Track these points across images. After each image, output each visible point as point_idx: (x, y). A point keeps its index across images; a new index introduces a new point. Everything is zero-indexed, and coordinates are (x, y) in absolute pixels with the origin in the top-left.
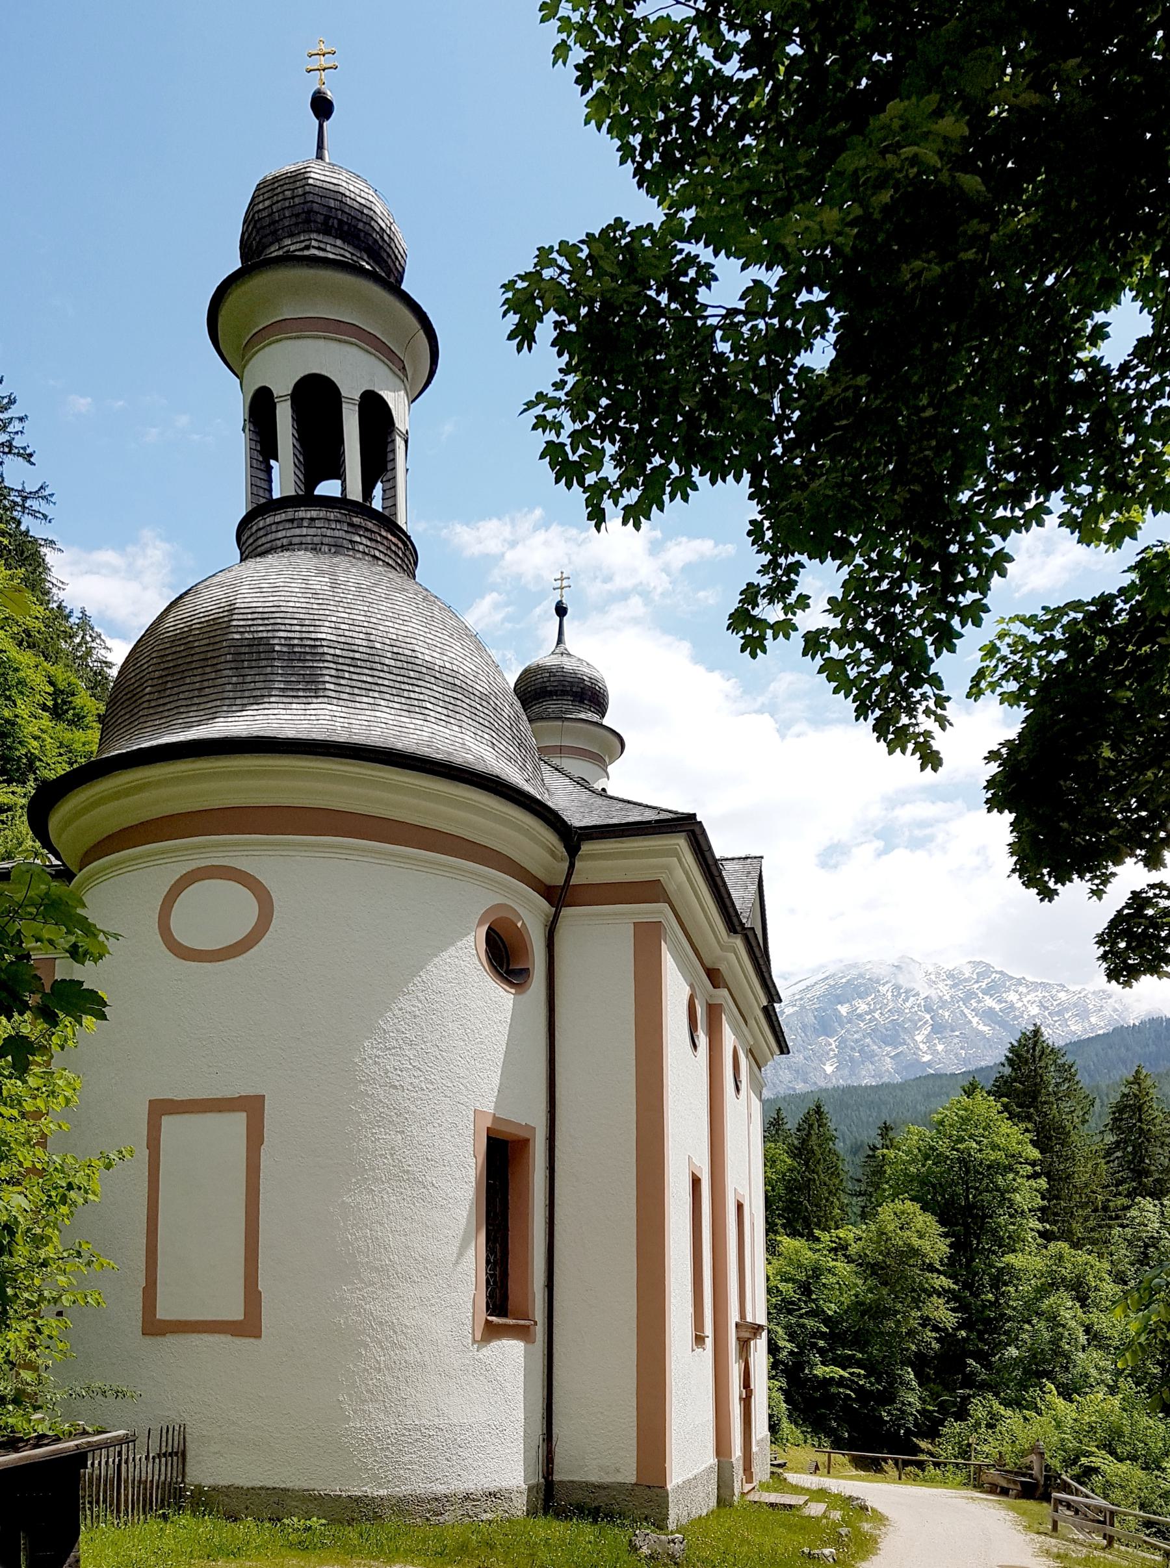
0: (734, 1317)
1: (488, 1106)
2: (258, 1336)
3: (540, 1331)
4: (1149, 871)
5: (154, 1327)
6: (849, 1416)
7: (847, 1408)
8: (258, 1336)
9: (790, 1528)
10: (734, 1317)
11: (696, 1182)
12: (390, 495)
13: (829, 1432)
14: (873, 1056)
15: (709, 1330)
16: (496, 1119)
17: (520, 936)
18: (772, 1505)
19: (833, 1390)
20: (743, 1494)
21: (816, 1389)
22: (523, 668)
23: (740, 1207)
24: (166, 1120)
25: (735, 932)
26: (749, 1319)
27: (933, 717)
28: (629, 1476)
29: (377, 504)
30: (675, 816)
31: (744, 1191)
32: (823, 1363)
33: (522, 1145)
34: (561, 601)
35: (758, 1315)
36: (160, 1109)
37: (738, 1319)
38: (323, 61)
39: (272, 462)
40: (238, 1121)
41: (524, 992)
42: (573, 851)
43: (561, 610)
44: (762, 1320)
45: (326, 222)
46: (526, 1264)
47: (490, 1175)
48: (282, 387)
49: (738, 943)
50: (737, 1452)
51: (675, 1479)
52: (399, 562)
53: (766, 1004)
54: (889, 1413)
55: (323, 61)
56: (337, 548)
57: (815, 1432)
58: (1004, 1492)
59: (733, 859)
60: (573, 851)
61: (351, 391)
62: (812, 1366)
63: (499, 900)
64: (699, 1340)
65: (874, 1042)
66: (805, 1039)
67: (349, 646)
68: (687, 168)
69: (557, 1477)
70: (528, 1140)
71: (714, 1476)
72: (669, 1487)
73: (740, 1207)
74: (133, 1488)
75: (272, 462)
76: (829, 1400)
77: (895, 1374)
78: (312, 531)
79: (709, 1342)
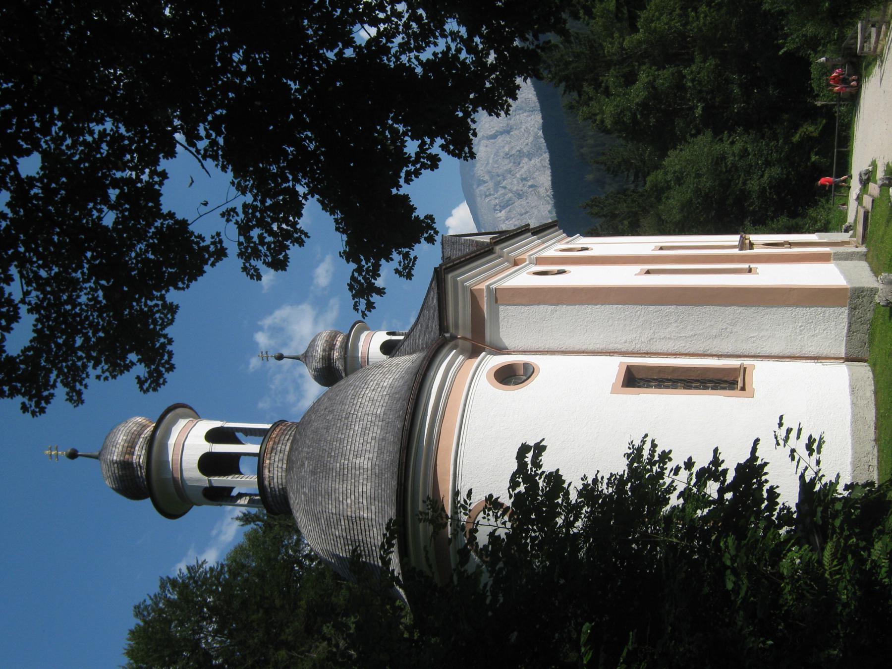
0: (736, 251)
3: (747, 362)
10: (736, 251)
11: (648, 272)
14: (530, 172)
15: (746, 266)
22: (313, 380)
23: (661, 248)
25: (493, 249)
26: (737, 243)
28: (844, 312)
30: (435, 279)
31: (653, 246)
34: (275, 357)
35: (735, 239)
37: (738, 249)
45: (129, 454)
52: (289, 428)
53: (530, 234)
59: (443, 252)
64: (750, 271)
65: (519, 171)
66: (517, 218)
68: (815, 175)
70: (628, 366)
71: (843, 263)
73: (661, 248)
77: (499, 509)
79: (752, 266)
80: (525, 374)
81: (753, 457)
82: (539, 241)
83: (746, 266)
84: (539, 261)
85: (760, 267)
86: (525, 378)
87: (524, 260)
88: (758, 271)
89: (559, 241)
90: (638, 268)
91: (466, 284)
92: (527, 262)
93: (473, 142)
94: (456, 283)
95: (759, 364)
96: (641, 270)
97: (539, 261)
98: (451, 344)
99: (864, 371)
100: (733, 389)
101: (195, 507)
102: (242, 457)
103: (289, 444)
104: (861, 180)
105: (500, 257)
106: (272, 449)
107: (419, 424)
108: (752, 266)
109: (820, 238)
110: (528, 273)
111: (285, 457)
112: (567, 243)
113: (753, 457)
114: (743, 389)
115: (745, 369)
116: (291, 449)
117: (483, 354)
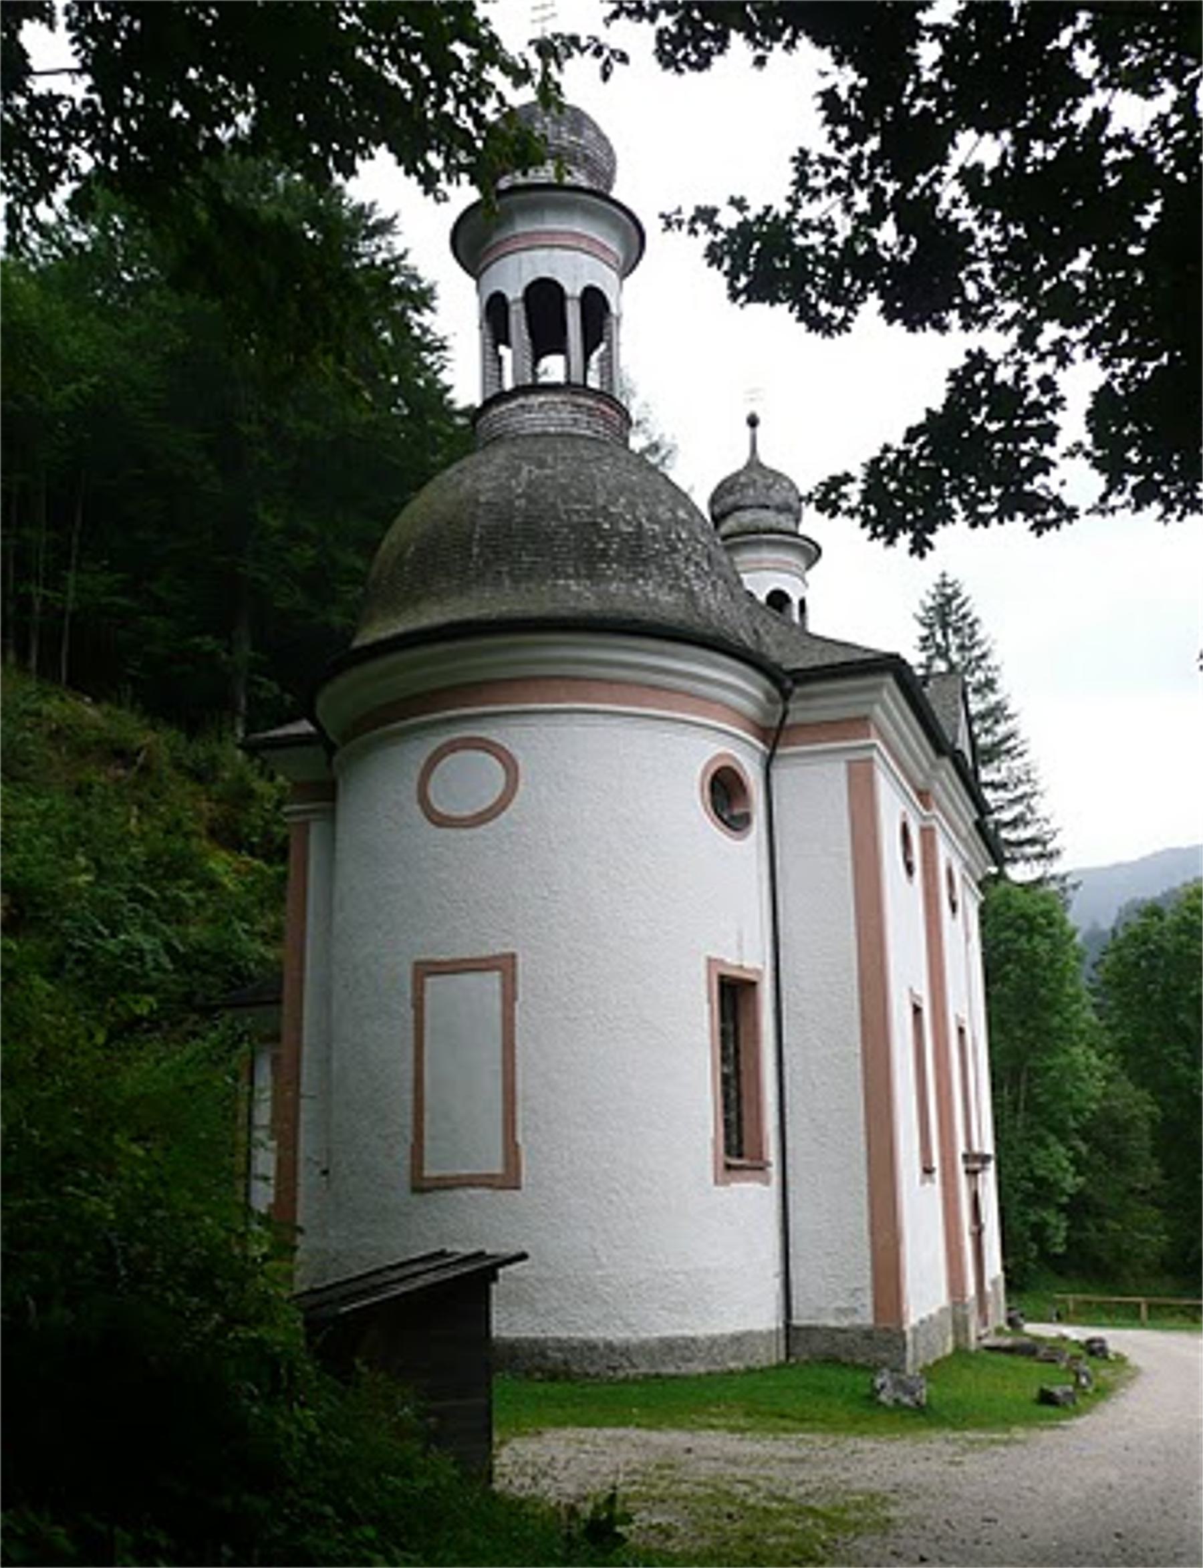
0: (961, 1148)
2: (513, 956)
3: (774, 1171)
4: (1094, 394)
5: (421, 1186)
8: (513, 956)
10: (961, 1148)
11: (917, 1010)
12: (608, 363)
15: (936, 1163)
20: (979, 1338)
23: (961, 1031)
24: (429, 980)
26: (976, 1148)
27: (851, 200)
28: (866, 1318)
29: (594, 382)
36: (425, 970)
38: (546, 13)
39: (503, 350)
40: (493, 981)
41: (745, 837)
42: (786, 695)
43: (753, 422)
44: (989, 1149)
47: (723, 1018)
48: (514, 293)
49: (946, 762)
50: (971, 1290)
51: (913, 1317)
55: (546, 13)
60: (786, 695)
61: (573, 289)
63: (722, 749)
64: (928, 1171)
69: (795, 1322)
72: (907, 1327)
73: (961, 1031)
74: (416, 1275)
75: (503, 350)
78: (541, 415)
79: (937, 1175)
80: (732, 817)
81: (392, 220)
82: (964, 832)
83: (936, 1163)
84: (927, 834)
85: (935, 1187)
86: (726, 816)
87: (927, 806)
88: (928, 1185)
89: (967, 866)
90: (924, 992)
91: (878, 709)
92: (925, 813)
93: (988, 137)
94: (877, 688)
95: (773, 1189)
96: (919, 998)
97: (927, 834)
98: (775, 693)
99: (774, 1354)
100: (728, 1152)
101: (472, 283)
102: (795, 1322)
103: (589, 433)
104: (1091, 1341)
105: (933, 766)
106: (579, 406)
107: (538, 227)
108: (937, 1175)
109: (994, 1283)
110: (904, 814)
111: (567, 429)
112: (963, 878)
113: (392, 220)
114: (729, 1167)
115: (761, 1169)
116: (582, 437)
117: (761, 746)
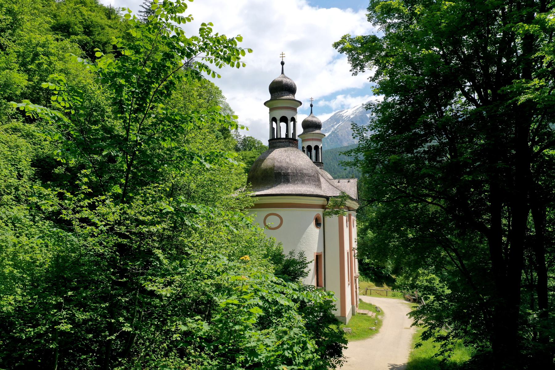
1: (316, 251)
6: (375, 274)
7: (373, 270)
9: (366, 320)
11: (348, 253)
13: (370, 277)
16: (317, 253)
17: (320, 218)
18: (362, 314)
19: (370, 266)
21: (366, 265)
32: (368, 259)
33: (321, 255)
46: (321, 280)
54: (384, 271)
56: (287, 146)
57: (366, 277)
58: (410, 300)
62: (365, 259)
67: (293, 173)
76: (369, 269)
